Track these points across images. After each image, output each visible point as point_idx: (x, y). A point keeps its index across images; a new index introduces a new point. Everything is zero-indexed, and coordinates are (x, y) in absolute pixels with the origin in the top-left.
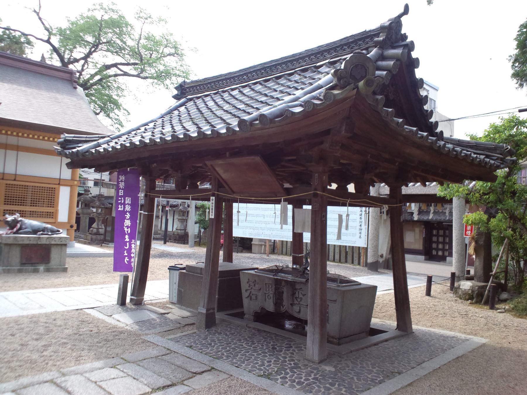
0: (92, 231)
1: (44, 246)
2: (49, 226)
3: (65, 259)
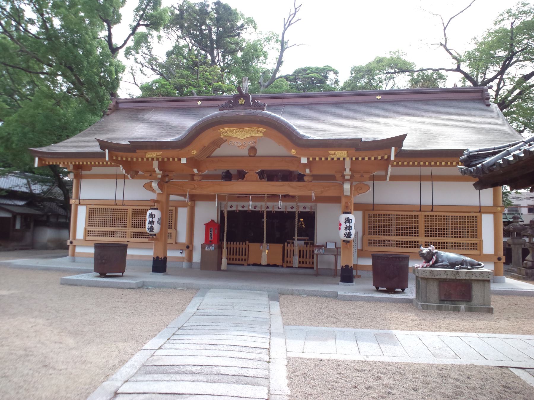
0: (526, 264)
1: (464, 281)
2: (468, 259)
3: (490, 298)
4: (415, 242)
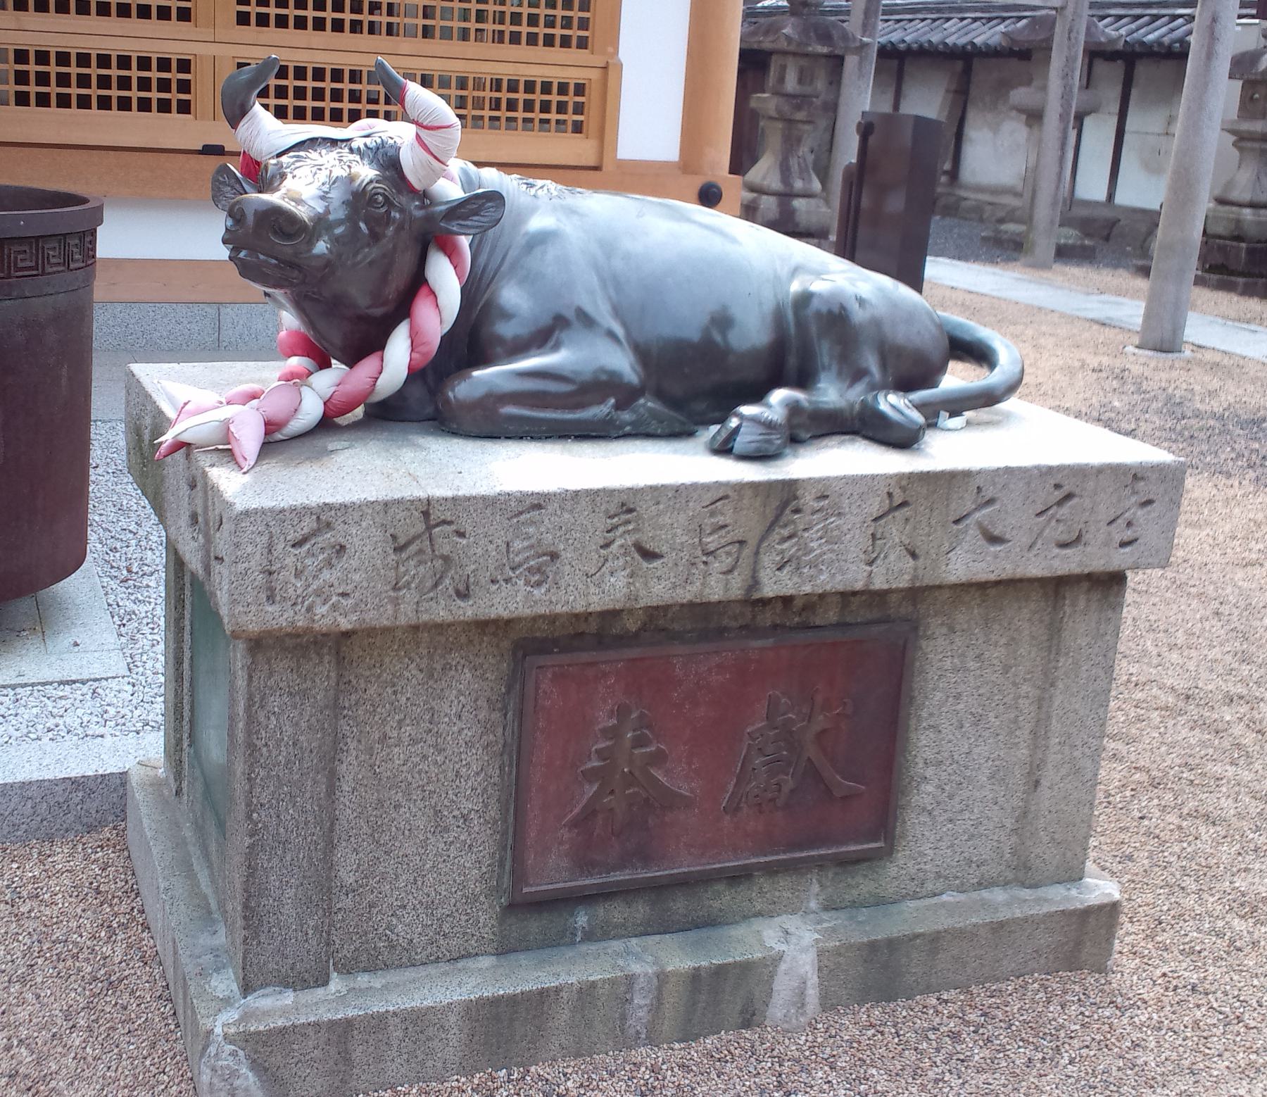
1: (831, 615)
4: (164, 64)
